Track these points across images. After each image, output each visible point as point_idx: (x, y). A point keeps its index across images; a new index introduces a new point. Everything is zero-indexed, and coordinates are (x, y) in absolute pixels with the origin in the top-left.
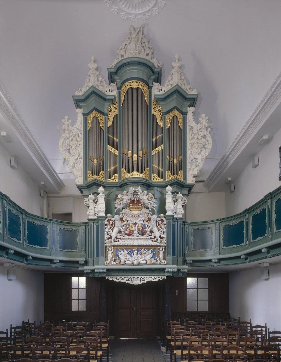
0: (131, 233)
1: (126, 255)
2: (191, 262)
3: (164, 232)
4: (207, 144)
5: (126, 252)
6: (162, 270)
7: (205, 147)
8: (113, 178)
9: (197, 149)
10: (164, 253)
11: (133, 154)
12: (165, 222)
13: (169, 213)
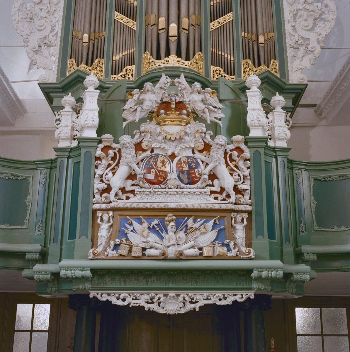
3: (244, 177)
4: (327, 12)
6: (244, 275)
7: (323, 17)
10: (248, 229)
12: (247, 153)
13: (254, 133)
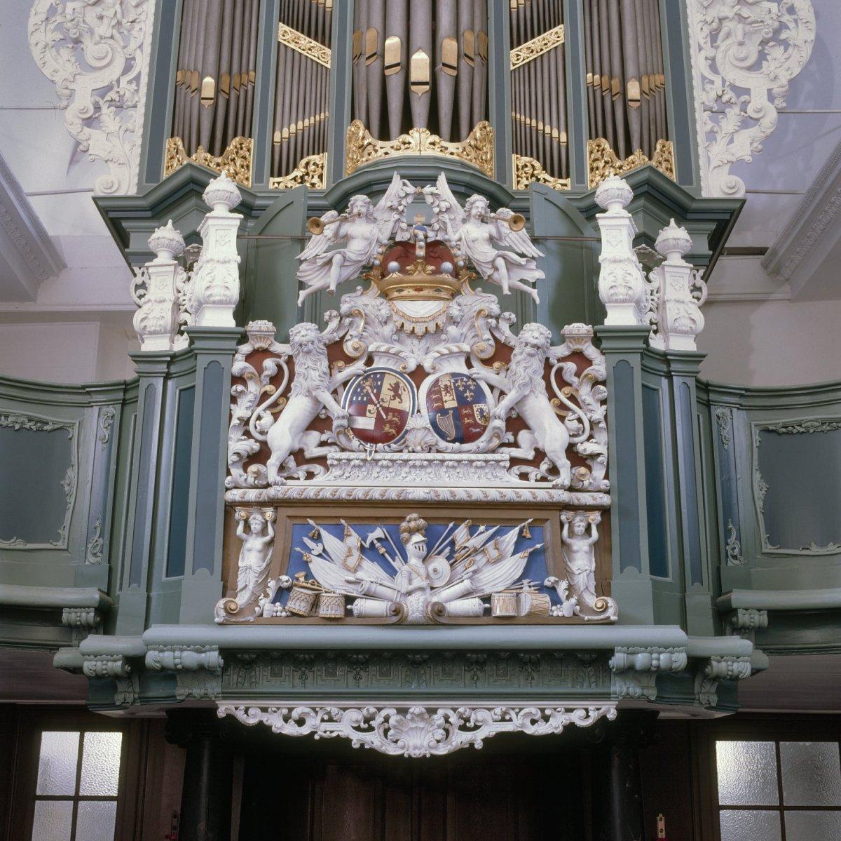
0: (387, 428)
1: (352, 561)
2: (763, 619)
3: (593, 424)
4: (792, 25)
5: (354, 540)
6: (591, 662)
7: (783, 36)
8: (298, 173)
9: (741, 44)
10: (601, 549)
11: (408, 51)
12: (600, 367)
13: (618, 317)
